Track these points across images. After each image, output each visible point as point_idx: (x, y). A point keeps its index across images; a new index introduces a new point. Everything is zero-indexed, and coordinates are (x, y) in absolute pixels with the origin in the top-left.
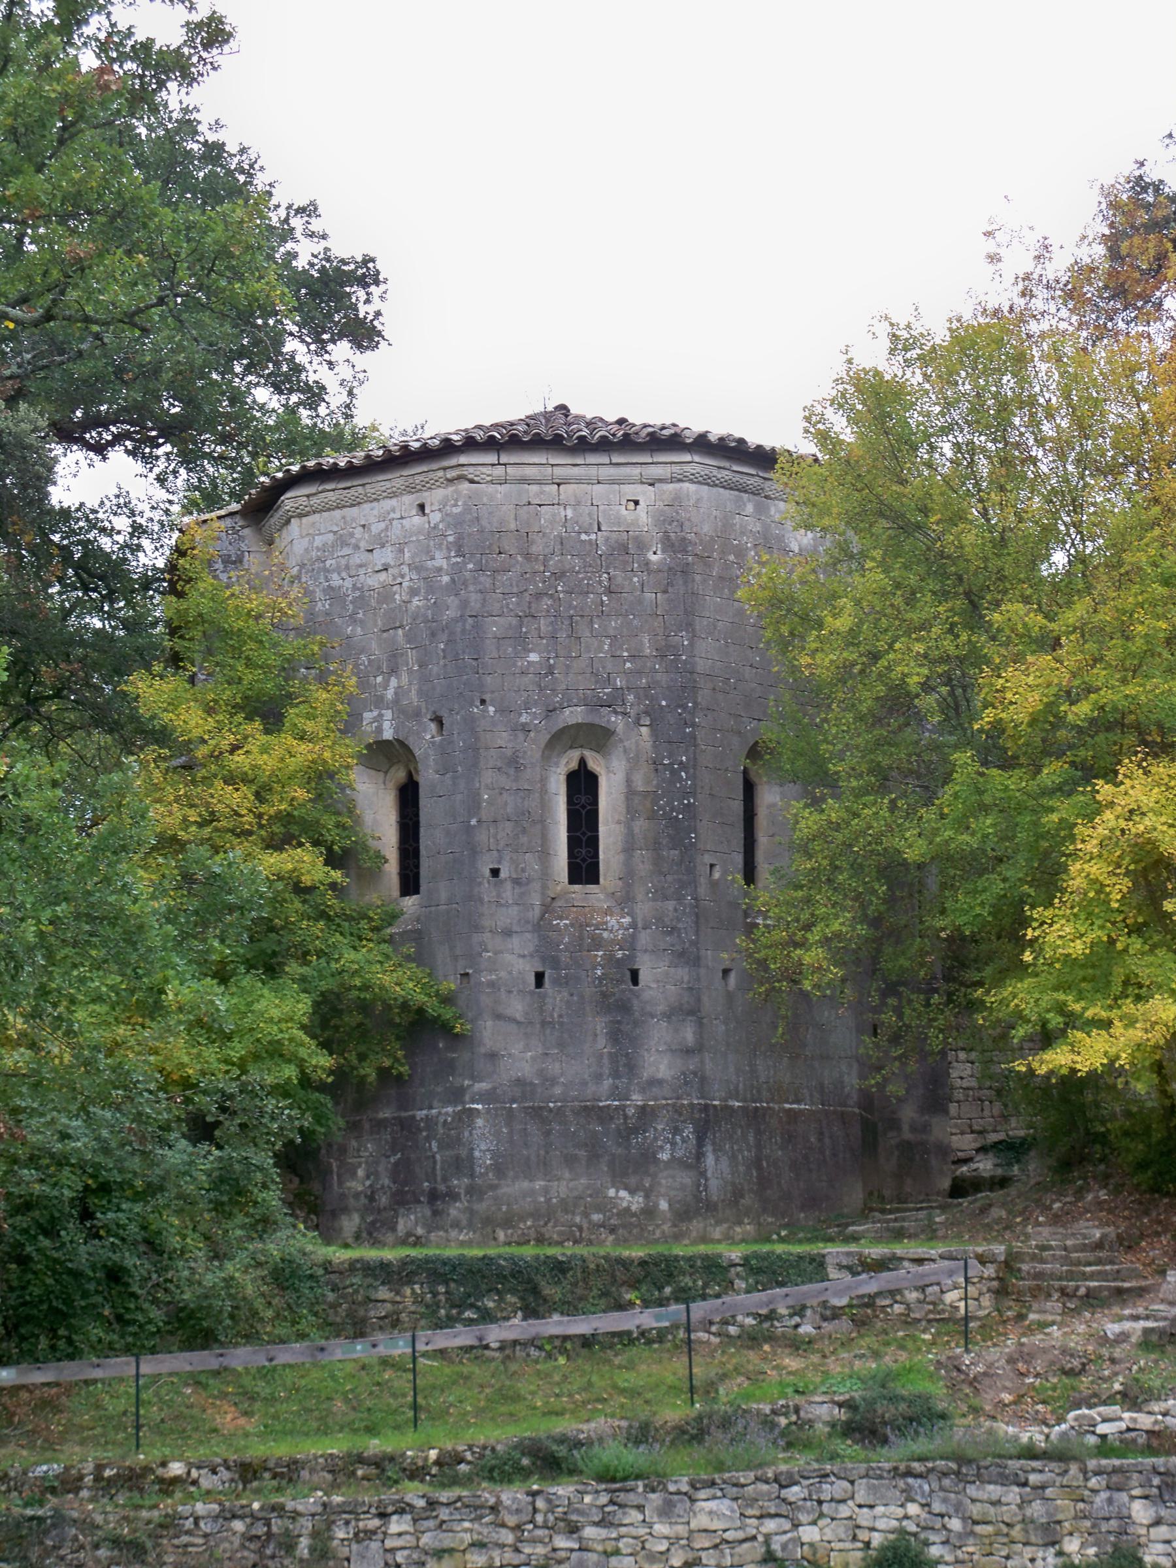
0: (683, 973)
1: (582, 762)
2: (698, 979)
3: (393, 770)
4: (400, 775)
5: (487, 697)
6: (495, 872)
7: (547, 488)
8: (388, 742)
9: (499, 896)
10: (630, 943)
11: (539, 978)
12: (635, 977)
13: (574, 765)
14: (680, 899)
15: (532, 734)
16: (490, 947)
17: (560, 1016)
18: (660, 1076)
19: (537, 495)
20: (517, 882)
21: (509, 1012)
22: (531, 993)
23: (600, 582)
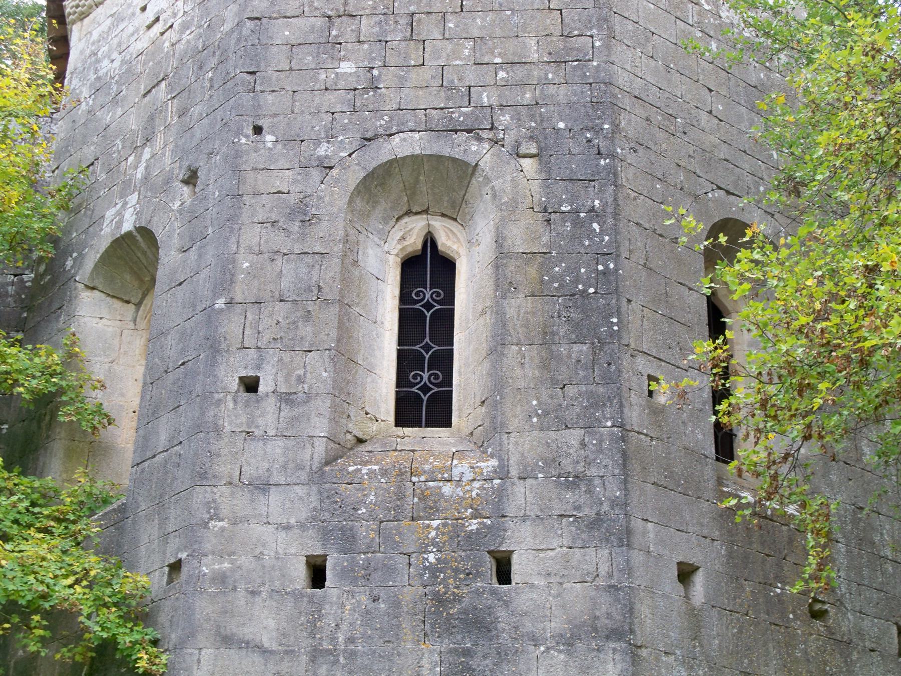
1: (430, 242)
2: (629, 570)
5: (265, 123)
6: (251, 385)
8: (129, 234)
13: (414, 243)
17: (351, 640)
20: (287, 399)
21: (248, 632)
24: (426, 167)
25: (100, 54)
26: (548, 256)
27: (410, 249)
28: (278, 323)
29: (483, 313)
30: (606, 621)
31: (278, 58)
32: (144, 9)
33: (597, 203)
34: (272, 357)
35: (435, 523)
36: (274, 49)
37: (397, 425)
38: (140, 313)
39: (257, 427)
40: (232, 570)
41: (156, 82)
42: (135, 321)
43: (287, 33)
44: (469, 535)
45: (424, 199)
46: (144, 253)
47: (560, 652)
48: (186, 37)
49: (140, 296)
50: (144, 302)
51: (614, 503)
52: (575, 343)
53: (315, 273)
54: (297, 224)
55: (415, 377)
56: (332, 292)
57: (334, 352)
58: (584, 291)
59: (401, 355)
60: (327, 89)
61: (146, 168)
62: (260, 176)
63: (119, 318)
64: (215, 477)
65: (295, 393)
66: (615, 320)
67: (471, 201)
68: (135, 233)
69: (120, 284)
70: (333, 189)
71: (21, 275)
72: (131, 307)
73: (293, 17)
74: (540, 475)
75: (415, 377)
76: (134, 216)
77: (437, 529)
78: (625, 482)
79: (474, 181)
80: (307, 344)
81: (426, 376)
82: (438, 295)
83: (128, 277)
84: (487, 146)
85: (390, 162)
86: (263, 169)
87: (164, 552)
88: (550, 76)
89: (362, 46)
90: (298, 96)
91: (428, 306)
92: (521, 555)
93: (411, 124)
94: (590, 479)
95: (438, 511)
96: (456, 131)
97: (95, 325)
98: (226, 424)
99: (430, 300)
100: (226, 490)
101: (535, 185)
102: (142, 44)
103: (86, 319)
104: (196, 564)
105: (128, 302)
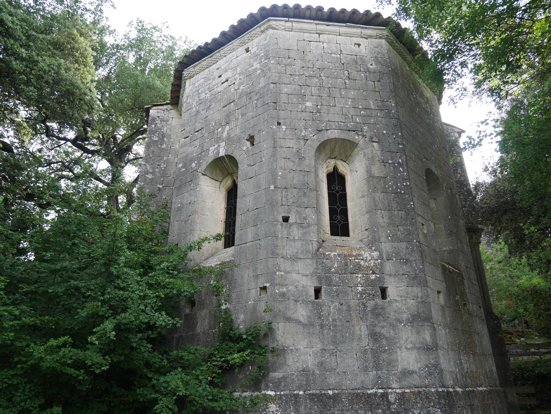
0: (416, 291)
1: (335, 168)
2: (427, 296)
3: (225, 181)
4: (228, 182)
5: (281, 121)
6: (286, 219)
7: (313, 35)
8: (222, 157)
9: (289, 234)
10: (379, 269)
11: (318, 292)
12: (384, 292)
13: (331, 169)
14: (410, 241)
15: (309, 142)
16: (282, 268)
17: (334, 320)
18: (411, 368)
19: (308, 37)
20: (301, 225)
21: (295, 316)
22: (313, 303)
23: (343, 74)
25: (200, 91)
27: (330, 171)
28: (294, 196)
29: (363, 197)
30: (423, 315)
31: (284, 98)
32: (220, 76)
33: (400, 160)
34: (294, 209)
35: (360, 275)
36: (282, 95)
37: (332, 235)
40: (288, 292)
41: (229, 102)
42: (219, 188)
43: (286, 90)
44: (372, 281)
45: (336, 154)
46: (227, 164)
47: (409, 326)
48: (242, 88)
51: (420, 270)
53: (306, 178)
54: (297, 160)
55: (335, 217)
56: (312, 186)
57: (316, 208)
58: (400, 192)
59: (330, 209)
60: (302, 111)
61: (228, 133)
62: (282, 141)
64: (277, 254)
66: (412, 203)
68: (225, 157)
72: (218, 183)
74: (394, 259)
75: (335, 217)
76: (225, 151)
77: (360, 278)
78: (423, 262)
79: (356, 149)
81: (339, 217)
82: (340, 188)
83: (218, 172)
84: (361, 137)
85: (328, 140)
87: (257, 282)
88: (379, 114)
90: (292, 113)
92: (391, 289)
93: (334, 127)
94: (411, 261)
95: (360, 271)
96: (350, 131)
100: (282, 260)
101: (379, 152)
102: (221, 88)
104: (273, 289)
105: (217, 181)
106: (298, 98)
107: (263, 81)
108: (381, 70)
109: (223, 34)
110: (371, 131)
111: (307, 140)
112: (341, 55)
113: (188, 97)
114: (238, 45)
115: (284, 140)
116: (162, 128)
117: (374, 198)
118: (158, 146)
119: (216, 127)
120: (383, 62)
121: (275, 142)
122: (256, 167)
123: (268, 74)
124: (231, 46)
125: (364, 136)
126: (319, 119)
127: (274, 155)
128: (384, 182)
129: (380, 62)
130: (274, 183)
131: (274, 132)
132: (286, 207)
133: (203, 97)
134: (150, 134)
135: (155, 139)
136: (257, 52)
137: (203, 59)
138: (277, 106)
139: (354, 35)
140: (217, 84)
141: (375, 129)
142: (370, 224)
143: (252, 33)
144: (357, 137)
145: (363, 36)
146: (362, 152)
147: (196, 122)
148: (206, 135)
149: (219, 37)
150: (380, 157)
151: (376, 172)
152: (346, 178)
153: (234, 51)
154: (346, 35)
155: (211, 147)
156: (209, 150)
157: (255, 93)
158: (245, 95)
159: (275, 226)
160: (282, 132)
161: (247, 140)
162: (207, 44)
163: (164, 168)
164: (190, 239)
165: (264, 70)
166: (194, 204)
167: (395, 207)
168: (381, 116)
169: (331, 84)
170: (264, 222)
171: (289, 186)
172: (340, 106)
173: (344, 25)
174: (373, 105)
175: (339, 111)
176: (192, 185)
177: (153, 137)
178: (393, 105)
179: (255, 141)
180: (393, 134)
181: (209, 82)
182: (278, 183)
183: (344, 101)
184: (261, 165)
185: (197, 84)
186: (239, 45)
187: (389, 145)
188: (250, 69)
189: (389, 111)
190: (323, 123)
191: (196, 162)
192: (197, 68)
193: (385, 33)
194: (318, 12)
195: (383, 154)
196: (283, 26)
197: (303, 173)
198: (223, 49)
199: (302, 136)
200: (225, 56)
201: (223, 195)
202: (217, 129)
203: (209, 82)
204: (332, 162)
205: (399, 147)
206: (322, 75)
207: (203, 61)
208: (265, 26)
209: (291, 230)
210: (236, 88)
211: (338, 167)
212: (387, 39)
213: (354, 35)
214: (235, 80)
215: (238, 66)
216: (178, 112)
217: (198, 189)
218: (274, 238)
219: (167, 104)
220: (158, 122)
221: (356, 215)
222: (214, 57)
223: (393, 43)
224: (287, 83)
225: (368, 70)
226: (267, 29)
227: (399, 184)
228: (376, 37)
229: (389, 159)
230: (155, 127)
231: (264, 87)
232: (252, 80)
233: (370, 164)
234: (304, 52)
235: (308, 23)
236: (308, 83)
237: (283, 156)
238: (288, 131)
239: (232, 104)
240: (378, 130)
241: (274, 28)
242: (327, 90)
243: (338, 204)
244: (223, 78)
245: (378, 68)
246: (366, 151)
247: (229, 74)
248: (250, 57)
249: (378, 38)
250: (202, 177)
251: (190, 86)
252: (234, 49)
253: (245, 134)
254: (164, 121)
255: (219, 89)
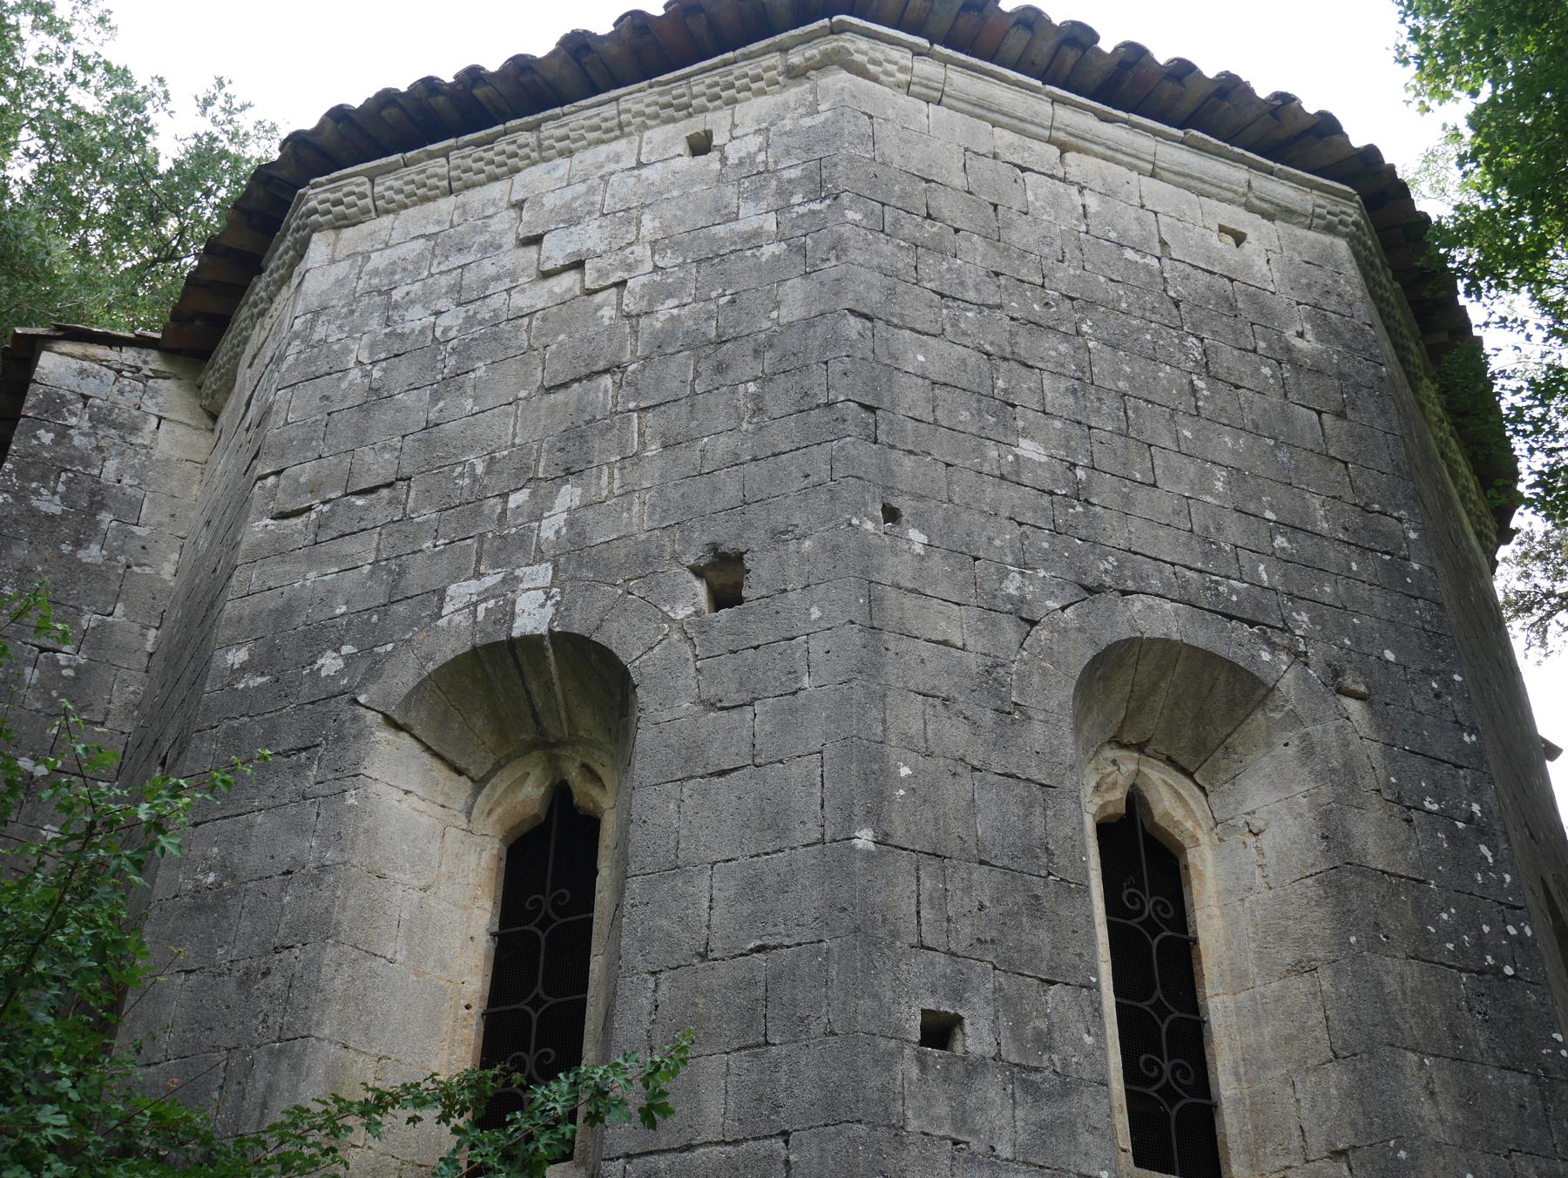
1: (1136, 800)
3: (500, 782)
6: (939, 1031)
7: (1037, 146)
8: (531, 642)
9: (962, 1119)
15: (1042, 633)
20: (1022, 1078)
23: (1182, 347)
24: (1179, 669)
25: (397, 295)
26: (1422, 886)
27: (1111, 810)
28: (981, 907)
29: (1303, 968)
31: (911, 397)
33: (1476, 808)
34: (985, 983)
38: (480, 799)
39: (974, 1132)
41: (584, 371)
42: (469, 814)
43: (921, 358)
46: (548, 687)
48: (666, 309)
49: (489, 766)
50: (493, 781)
52: (1508, 1069)
53: (1037, 819)
54: (990, 714)
58: (1498, 971)
60: (1002, 477)
61: (570, 524)
62: (909, 602)
63: (440, 800)
65: (1037, 1070)
67: (1240, 749)
68: (547, 643)
69: (457, 733)
70: (1043, 664)
71: (55, 651)
72: (465, 784)
73: (927, 334)
76: (549, 610)
79: (1259, 715)
80: (1044, 967)
81: (1167, 1066)
83: (479, 722)
84: (1284, 657)
85: (1130, 642)
86: (911, 591)
88: (1354, 567)
89: (1050, 421)
91: (1150, 924)
96: (1231, 618)
97: (396, 803)
98: (909, 1114)
99: (1154, 916)
101: (1375, 749)
103: (380, 788)
105: (459, 772)
106: (979, 410)
107: (799, 295)
108: (1346, 368)
109: (577, 45)
110: (1327, 639)
111: (1033, 623)
112: (1165, 261)
113: (317, 314)
114: (408, 188)
115: (922, 601)
116: (95, 456)
117: (1380, 984)
118: (56, 546)
119: (496, 484)
120: (1348, 336)
121: (874, 602)
122: (759, 720)
123: (832, 269)
124: (608, 111)
125: (1297, 655)
126: (1083, 533)
127: (870, 668)
128: (1417, 903)
129: (1337, 334)
130: (874, 816)
131: (867, 551)
132: (941, 959)
133: (417, 325)
134: (21, 472)
135: (50, 505)
136: (761, 157)
137: (430, 147)
138: (882, 427)
139: (1214, 190)
140: (512, 274)
141: (1343, 630)
142: (1361, 1122)
143: (737, 69)
144: (1266, 656)
145: (1257, 202)
146: (1293, 736)
147: (361, 444)
148: (428, 514)
149: (553, 54)
150: (1381, 773)
151: (1372, 849)
152: (1192, 856)
153: (623, 135)
154: (1180, 179)
155: (455, 580)
156: (441, 594)
157: (748, 347)
158: (689, 347)
159: (887, 1061)
160: (907, 557)
161: (698, 572)
162: (473, 75)
163: (78, 668)
164: (270, 1087)
165: (803, 246)
166: (317, 881)
167: (1483, 1045)
168: (1364, 577)
169: (1130, 379)
170: (816, 1028)
171: (953, 847)
172: (1176, 490)
173: (1180, 133)
174: (1326, 517)
175: (1177, 513)
176: (313, 773)
177: (36, 492)
178: (1413, 535)
179: (752, 578)
180: (1427, 673)
181: (456, 260)
182: (897, 820)
183: (1192, 469)
184: (793, 711)
185: (378, 260)
186: (656, 116)
187: (1416, 724)
188: (720, 231)
189: (1397, 566)
190: (1103, 557)
191: (347, 649)
192: (390, 181)
193: (1352, 212)
194: (1065, 49)
195: (1393, 760)
196: (903, 69)
197: (1020, 789)
198: (557, 117)
199: (1009, 598)
200: (570, 153)
201: (486, 856)
202: (504, 496)
203: (456, 260)
204: (1129, 762)
205: (1461, 740)
206: (1085, 328)
207: (432, 156)
208: (813, 51)
209: (972, 1101)
210: (631, 304)
211: (1151, 796)
212: (1355, 242)
213: (1214, 190)
214: (630, 267)
215: (644, 206)
216: (199, 396)
217: (351, 801)
218: (882, 1133)
219: (141, 343)
220: (78, 420)
221: (1265, 1066)
222: (501, 145)
223: (1372, 265)
224: (926, 327)
225: (1286, 356)
226: (822, 65)
227: (1486, 929)
228: (1312, 221)
229: (1425, 792)
230: (55, 442)
231: (809, 323)
232: (730, 284)
233: (1338, 799)
234: (995, 206)
235: (1016, 84)
236: (1022, 352)
237: (919, 680)
238: (937, 557)
239: (607, 381)
240: (1358, 641)
241: (860, 71)
242: (1110, 403)
243: (1158, 992)
244: (556, 250)
245: (1330, 356)
246: (1315, 730)
247: (590, 236)
248: (720, 178)
249: (1317, 229)
250: (384, 735)
251: (333, 261)
252: (621, 126)
253: (687, 541)
254: (112, 425)
255: (520, 301)
